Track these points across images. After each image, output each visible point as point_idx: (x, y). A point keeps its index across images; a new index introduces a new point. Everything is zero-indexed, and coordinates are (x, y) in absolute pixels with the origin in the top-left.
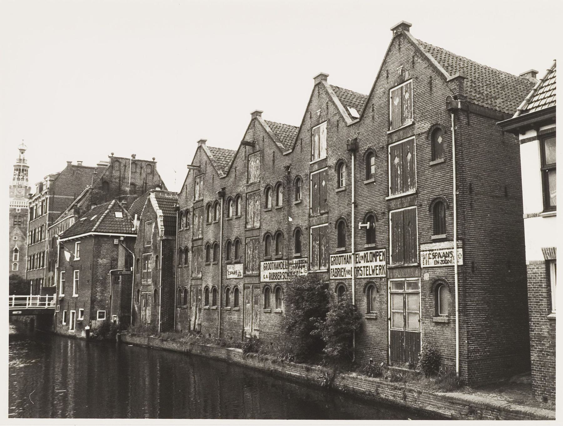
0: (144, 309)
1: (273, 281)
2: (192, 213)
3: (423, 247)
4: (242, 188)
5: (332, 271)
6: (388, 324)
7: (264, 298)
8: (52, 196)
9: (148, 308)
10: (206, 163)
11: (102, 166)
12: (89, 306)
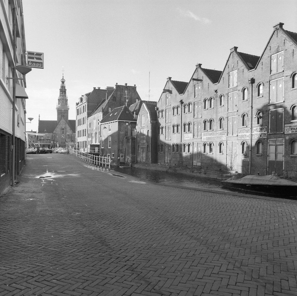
3: (286, 125)
5: (239, 136)
6: (267, 158)
12: (117, 152)
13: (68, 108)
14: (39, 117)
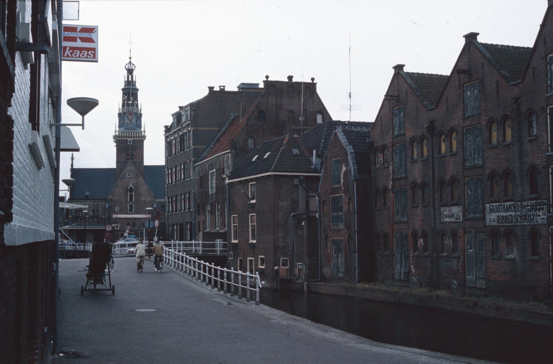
0: (335, 255)
1: (502, 224)
2: (390, 149)
4: (457, 121)
7: (491, 243)
8: (195, 128)
9: (340, 255)
10: (407, 92)
11: (247, 90)
13: (143, 134)
14: (72, 161)
